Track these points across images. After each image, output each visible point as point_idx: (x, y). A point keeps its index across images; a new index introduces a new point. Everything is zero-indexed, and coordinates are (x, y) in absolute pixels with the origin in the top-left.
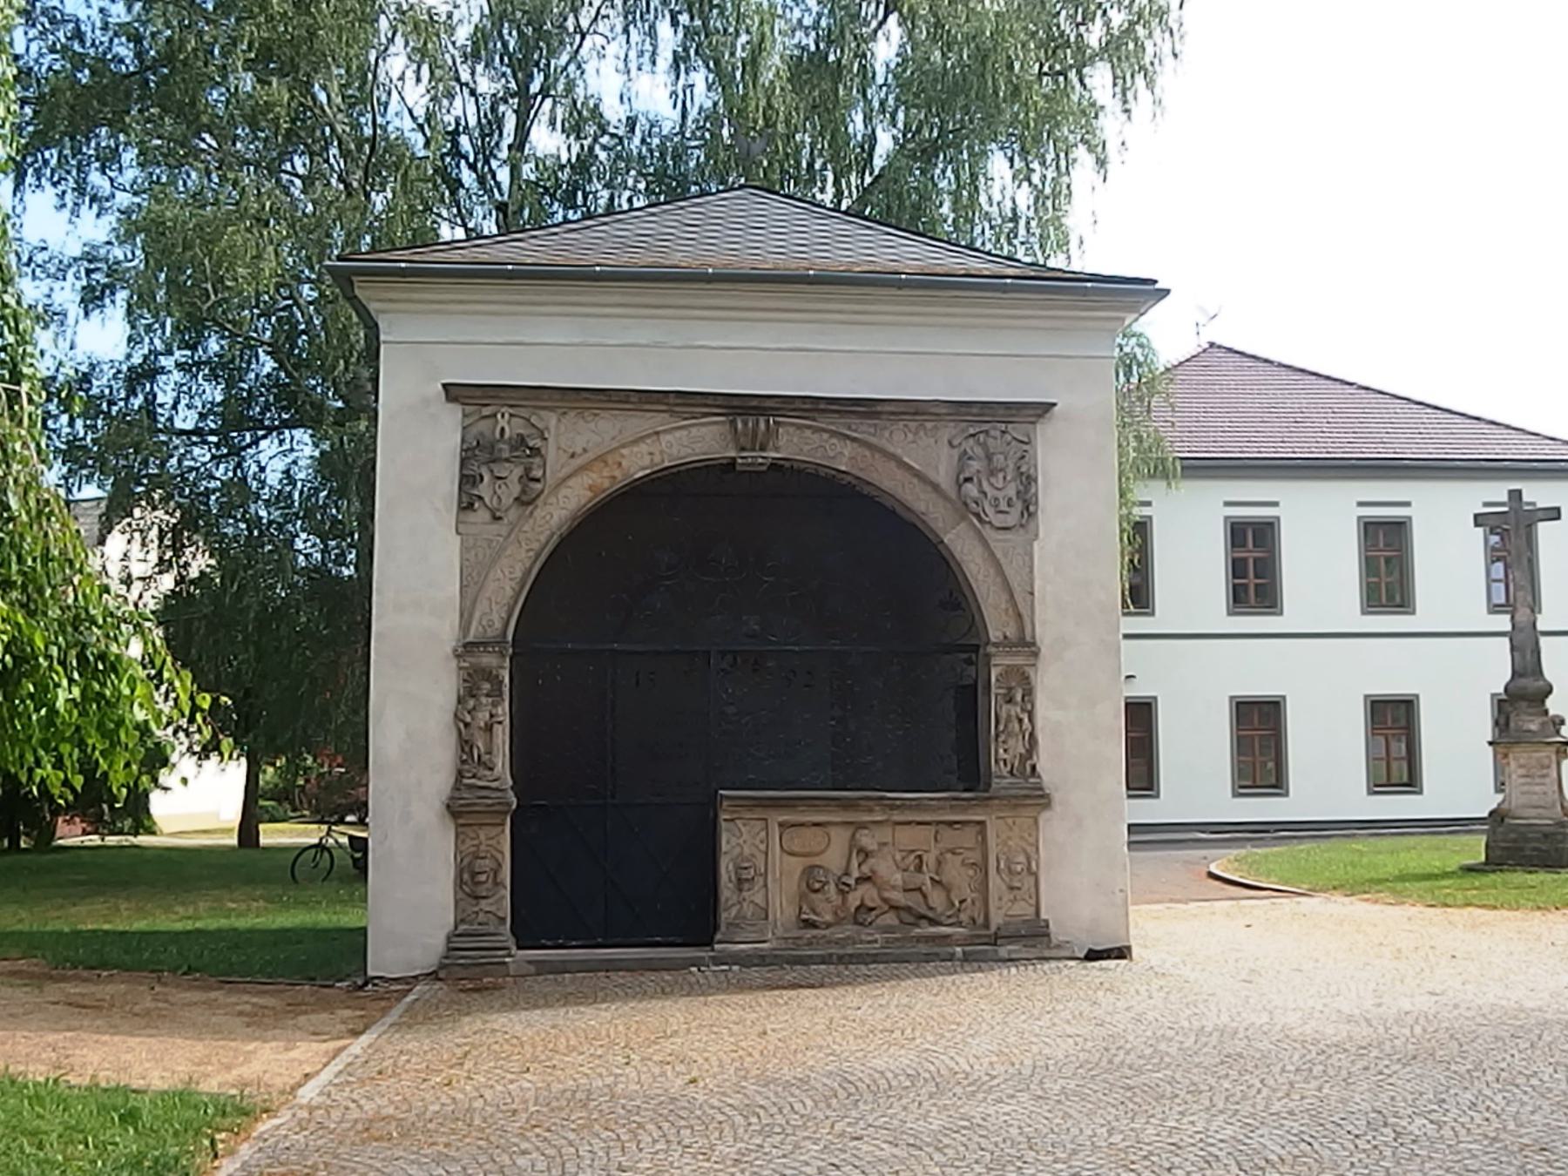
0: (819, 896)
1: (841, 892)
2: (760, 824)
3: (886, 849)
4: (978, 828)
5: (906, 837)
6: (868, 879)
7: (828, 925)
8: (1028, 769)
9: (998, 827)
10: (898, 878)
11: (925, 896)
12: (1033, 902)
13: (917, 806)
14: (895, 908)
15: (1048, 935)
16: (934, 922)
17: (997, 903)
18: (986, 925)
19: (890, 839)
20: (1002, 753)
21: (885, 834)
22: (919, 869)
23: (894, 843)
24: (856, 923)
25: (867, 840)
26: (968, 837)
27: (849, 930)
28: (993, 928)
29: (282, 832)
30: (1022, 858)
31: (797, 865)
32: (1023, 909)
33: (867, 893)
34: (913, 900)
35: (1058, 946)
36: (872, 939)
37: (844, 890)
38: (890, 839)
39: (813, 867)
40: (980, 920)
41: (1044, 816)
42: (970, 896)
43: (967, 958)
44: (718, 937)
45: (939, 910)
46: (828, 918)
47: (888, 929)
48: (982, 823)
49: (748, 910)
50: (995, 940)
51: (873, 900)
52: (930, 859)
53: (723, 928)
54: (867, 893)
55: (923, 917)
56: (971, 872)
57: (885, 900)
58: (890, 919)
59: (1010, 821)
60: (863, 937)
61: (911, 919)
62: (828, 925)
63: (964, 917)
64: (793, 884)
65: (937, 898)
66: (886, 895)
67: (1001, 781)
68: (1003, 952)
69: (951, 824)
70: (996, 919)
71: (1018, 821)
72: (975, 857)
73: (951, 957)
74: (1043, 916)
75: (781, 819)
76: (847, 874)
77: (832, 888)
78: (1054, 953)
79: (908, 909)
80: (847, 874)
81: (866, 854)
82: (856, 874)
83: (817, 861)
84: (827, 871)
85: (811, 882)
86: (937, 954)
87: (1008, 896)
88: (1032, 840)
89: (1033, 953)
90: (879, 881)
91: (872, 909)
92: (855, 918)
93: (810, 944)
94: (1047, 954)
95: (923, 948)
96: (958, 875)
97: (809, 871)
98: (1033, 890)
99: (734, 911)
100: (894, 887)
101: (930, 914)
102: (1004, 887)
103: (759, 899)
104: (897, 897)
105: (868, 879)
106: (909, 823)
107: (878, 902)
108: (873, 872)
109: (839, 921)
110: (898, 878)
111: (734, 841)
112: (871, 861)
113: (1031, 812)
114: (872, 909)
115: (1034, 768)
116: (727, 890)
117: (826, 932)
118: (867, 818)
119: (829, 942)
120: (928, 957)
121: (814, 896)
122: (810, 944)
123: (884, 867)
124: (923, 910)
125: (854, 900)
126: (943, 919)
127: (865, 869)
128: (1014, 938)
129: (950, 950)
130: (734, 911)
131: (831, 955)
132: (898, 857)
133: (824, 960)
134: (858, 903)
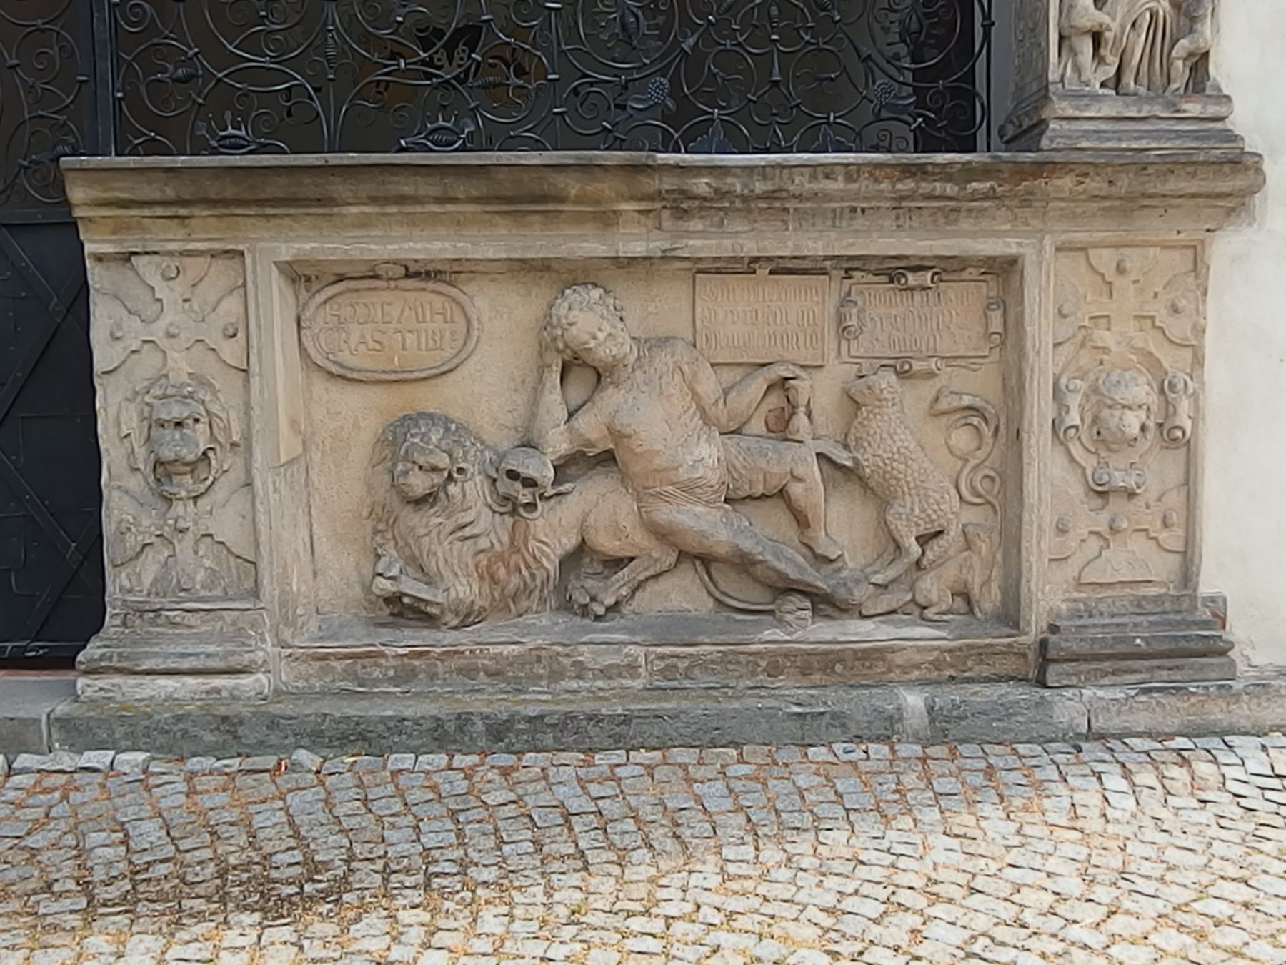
0: (432, 518)
1: (511, 506)
2: (221, 274)
3: (664, 360)
4: (989, 288)
5: (745, 318)
6: (608, 458)
7: (469, 617)
8: (1180, 69)
9: (1069, 283)
10: (706, 456)
11: (801, 520)
12: (1174, 539)
13: (775, 204)
14: (705, 560)
15: (1221, 650)
16: (825, 604)
17: (1049, 542)
18: (1010, 616)
19: (680, 325)
20: (997, 79)
21: (665, 307)
22: (781, 428)
23: (685, 334)
24: (567, 606)
25: (590, 321)
26: (953, 318)
27: (542, 629)
28: (1030, 638)
29: (1032, 379)
30: (1141, 390)
31: (359, 414)
32: (1138, 562)
33: (596, 508)
34: (762, 534)
35: (1262, 688)
36: (612, 660)
37: (516, 495)
38: (680, 325)
39: (409, 421)
40: (990, 599)
41: (1226, 247)
42: (956, 516)
43: (943, 729)
44: (92, 651)
45: (852, 563)
46: (465, 590)
47: (674, 629)
48: (1004, 270)
49: (195, 564)
50: (1041, 666)
51: (617, 531)
52: (820, 394)
53: (111, 623)
54: (596, 508)
55: (786, 588)
56: (962, 439)
57: (662, 534)
58: (683, 594)
59: (1105, 260)
60: (585, 654)
61: (754, 595)
62: (469, 617)
63: (932, 588)
64: (346, 482)
65: (843, 527)
66: (664, 513)
67: (1082, 105)
68: (1069, 707)
69: (894, 271)
70: (1047, 596)
71: (1134, 259)
72: (975, 385)
73: (887, 729)
74: (1207, 586)
75: (286, 252)
76: (529, 444)
77: (473, 492)
78: (1242, 713)
79: (744, 564)
80: (529, 444)
81: (582, 370)
82: (558, 443)
83: (428, 399)
84: (455, 430)
85: (409, 480)
86: (839, 720)
87: (1087, 519)
88: (1180, 328)
89: (1172, 711)
90: (636, 468)
91: (617, 563)
92: (561, 588)
93: (405, 675)
94: (1217, 713)
95: (791, 693)
96: (920, 448)
97: (396, 439)
98: (1175, 499)
99: (149, 569)
100: (690, 489)
101: (820, 580)
102: (1077, 490)
103: (228, 527)
104: (707, 522)
105: (608, 458)
106: (749, 266)
107: (640, 540)
108: (617, 435)
109: (506, 603)
110: (706, 456)
111: (135, 331)
112: (611, 398)
113: (1186, 228)
114: (617, 563)
115: (1199, 63)
116: (123, 504)
117: (464, 639)
118: (589, 245)
119: (469, 672)
120: (806, 730)
121: (413, 519)
122: (405, 675)
123: (662, 420)
124: (793, 565)
125: (553, 530)
126: (860, 593)
127: (591, 426)
128: (1112, 658)
129: (878, 699)
130: (149, 569)
131: (463, 720)
132: (709, 385)
133: (442, 736)
134: (570, 542)
